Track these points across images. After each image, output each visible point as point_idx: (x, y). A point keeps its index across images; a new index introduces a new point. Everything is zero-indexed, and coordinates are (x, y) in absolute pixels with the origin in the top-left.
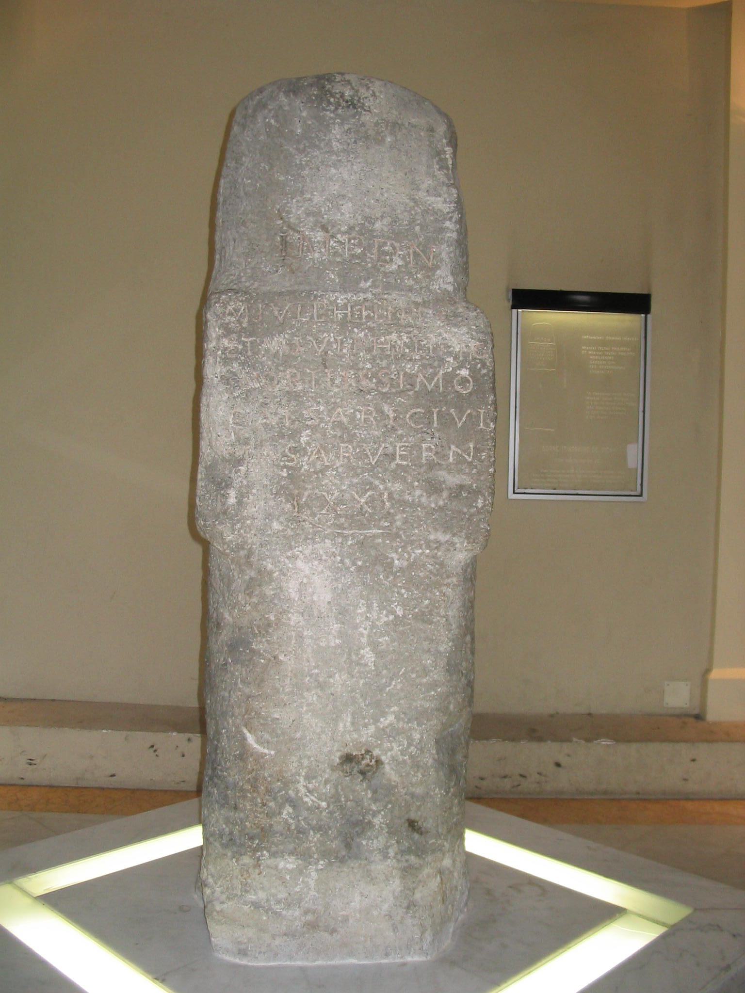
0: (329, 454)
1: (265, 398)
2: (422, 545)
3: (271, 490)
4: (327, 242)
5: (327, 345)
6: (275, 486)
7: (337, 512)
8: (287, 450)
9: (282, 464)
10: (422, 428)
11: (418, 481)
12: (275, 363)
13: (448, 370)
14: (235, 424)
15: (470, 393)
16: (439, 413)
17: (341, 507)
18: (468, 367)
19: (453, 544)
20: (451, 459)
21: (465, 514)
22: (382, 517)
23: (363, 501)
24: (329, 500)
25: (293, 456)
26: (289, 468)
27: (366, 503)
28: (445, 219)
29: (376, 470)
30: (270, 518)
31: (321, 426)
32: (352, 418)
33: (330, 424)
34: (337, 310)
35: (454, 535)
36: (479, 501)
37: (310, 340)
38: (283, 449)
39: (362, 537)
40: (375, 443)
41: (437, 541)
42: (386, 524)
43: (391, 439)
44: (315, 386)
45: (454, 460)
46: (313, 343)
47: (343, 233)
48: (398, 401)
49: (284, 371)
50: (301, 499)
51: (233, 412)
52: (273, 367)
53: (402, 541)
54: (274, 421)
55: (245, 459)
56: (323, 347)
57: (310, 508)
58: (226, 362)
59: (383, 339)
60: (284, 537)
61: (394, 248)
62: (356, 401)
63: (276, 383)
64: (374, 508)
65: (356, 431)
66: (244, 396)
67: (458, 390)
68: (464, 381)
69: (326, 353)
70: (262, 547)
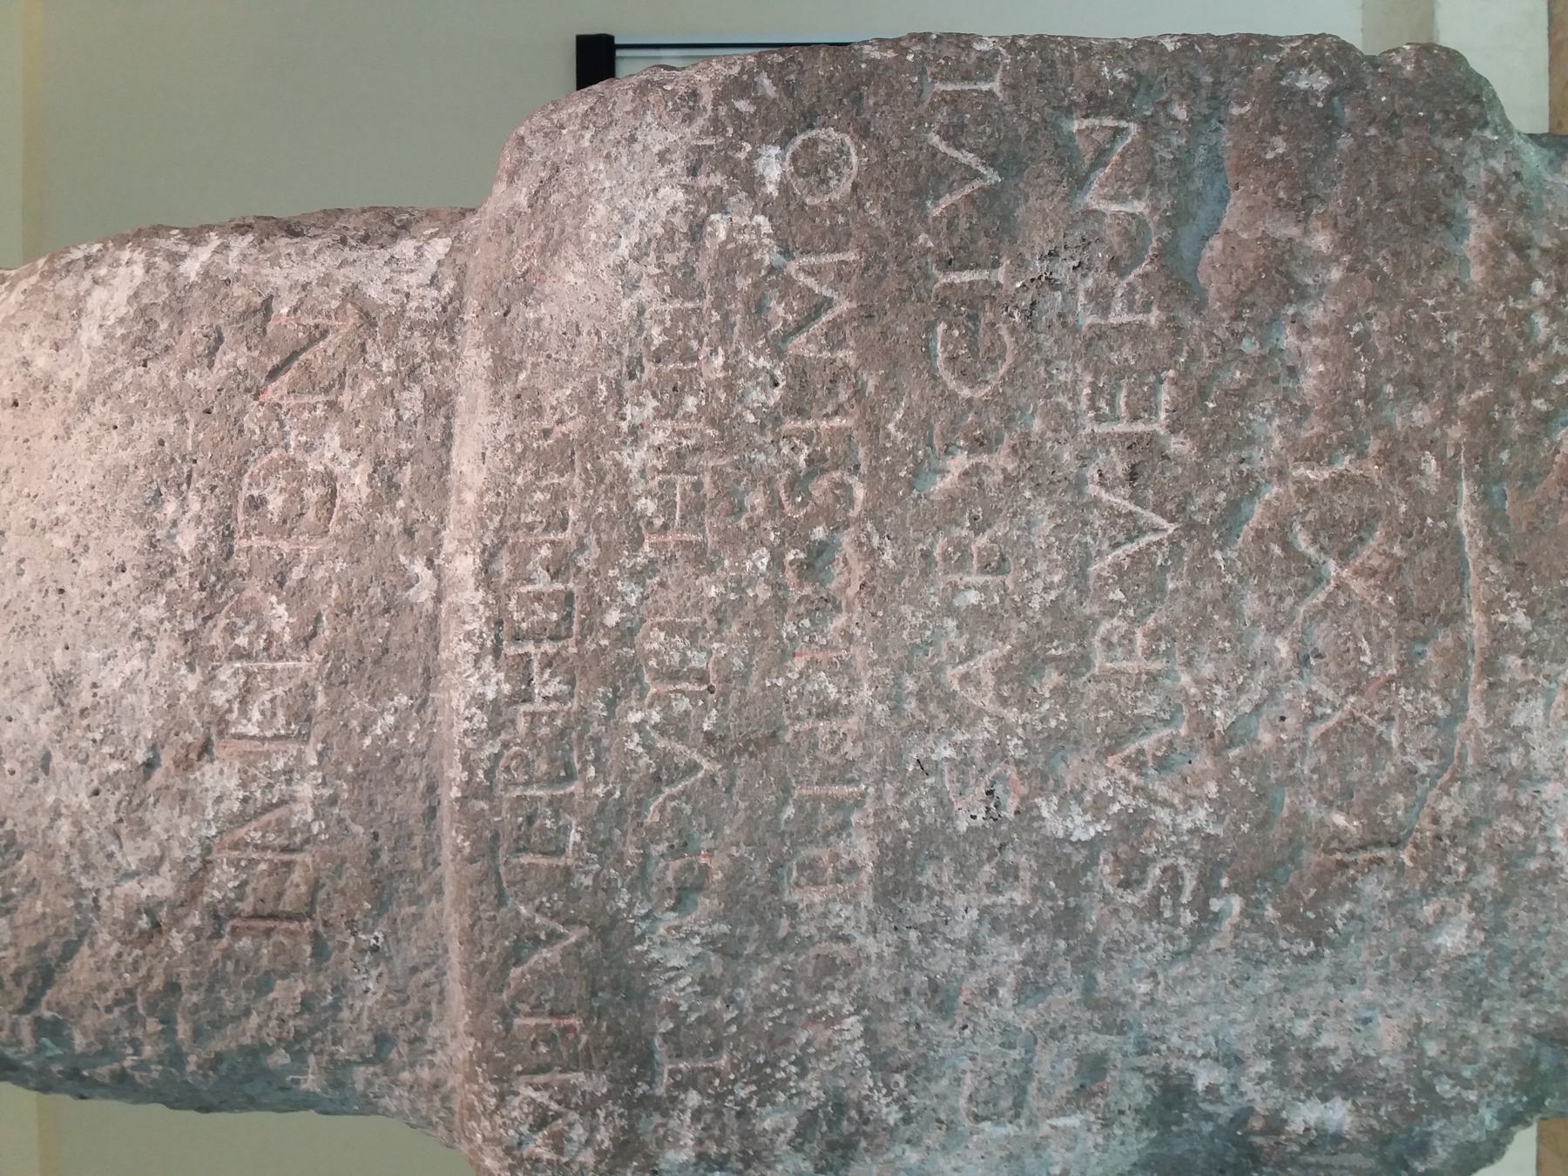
0: (1141, 717)
1: (906, 991)
2: (1512, 312)
3: (1299, 959)
4: (246, 746)
5: (681, 736)
6: (1283, 944)
7: (1391, 680)
8: (1131, 899)
9: (1188, 918)
10: (1013, 330)
11: (1238, 337)
12: (757, 953)
13: (767, 228)
14: (1017, 1116)
15: (863, 132)
16: (947, 265)
17: (1366, 659)
18: (749, 148)
19: (1496, 183)
20: (1139, 207)
21: (1362, 143)
22: (1405, 484)
23: (1332, 566)
24: (1338, 715)
25: (1155, 872)
26: (1208, 887)
27: (1344, 556)
28: (171, 278)
29: (1199, 518)
30: (1418, 960)
31: (1019, 754)
32: (984, 620)
33: (1012, 715)
34: (528, 699)
35: (1458, 182)
36: (1302, 85)
37: (662, 809)
38: (1127, 915)
39: (1494, 568)
40: (1085, 523)
41: (1494, 255)
42: (1431, 465)
43: (1066, 456)
44: (850, 782)
45: (1137, 195)
46: (672, 797)
47: (210, 679)
48: (900, 436)
49: (792, 910)
50: (1338, 834)
51: (968, 1123)
52: (777, 961)
53: (1499, 396)
54: (1006, 954)
55: (1166, 1068)
56: (684, 752)
57: (1380, 795)
58: (757, 1155)
59: (648, 506)
60: (1503, 901)
61: (272, 470)
62: (906, 610)
63: (841, 947)
64: (1366, 523)
65: (1036, 603)
66: (900, 1079)
67: (847, 186)
68: (813, 167)
69: (709, 738)
70: (1540, 990)
